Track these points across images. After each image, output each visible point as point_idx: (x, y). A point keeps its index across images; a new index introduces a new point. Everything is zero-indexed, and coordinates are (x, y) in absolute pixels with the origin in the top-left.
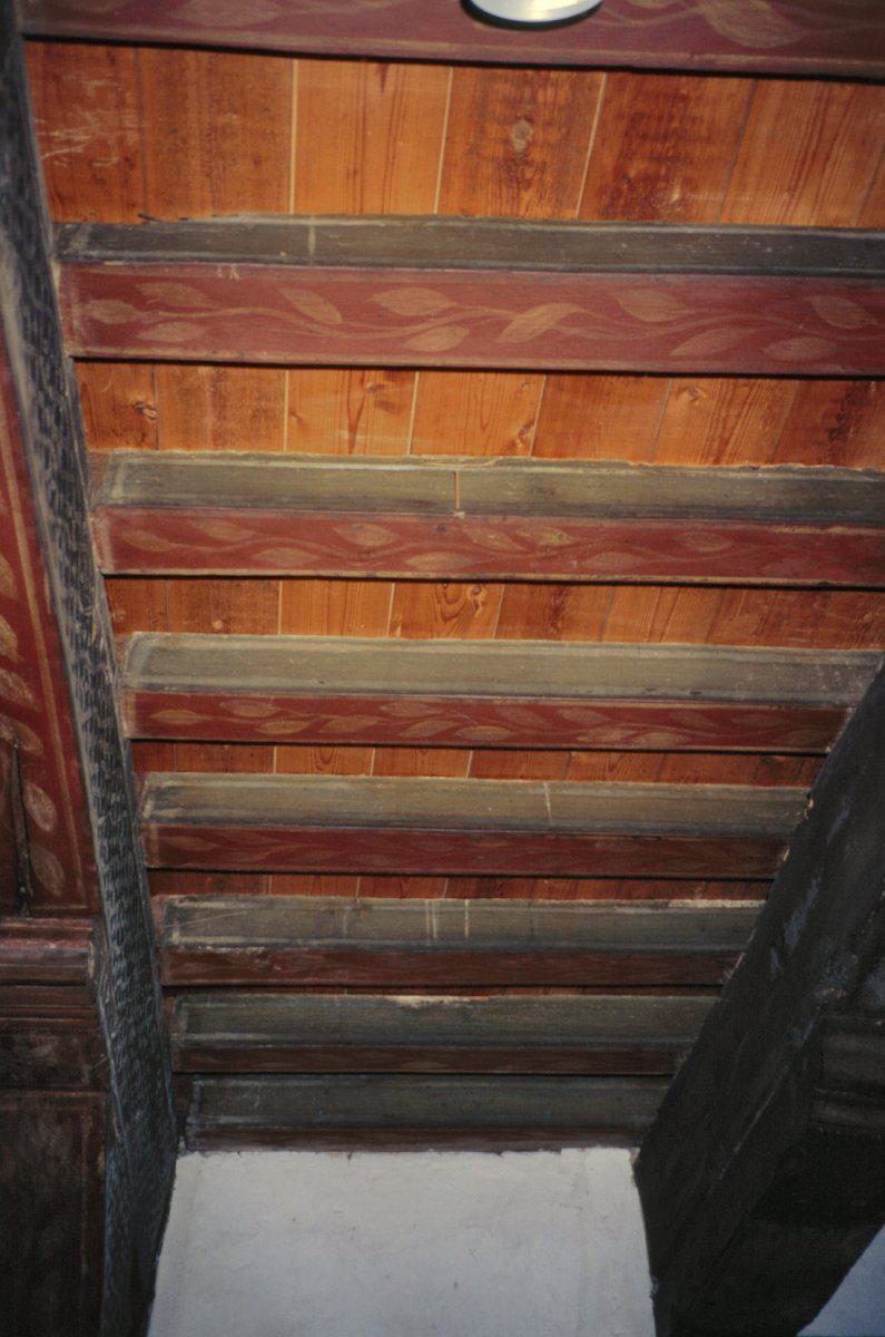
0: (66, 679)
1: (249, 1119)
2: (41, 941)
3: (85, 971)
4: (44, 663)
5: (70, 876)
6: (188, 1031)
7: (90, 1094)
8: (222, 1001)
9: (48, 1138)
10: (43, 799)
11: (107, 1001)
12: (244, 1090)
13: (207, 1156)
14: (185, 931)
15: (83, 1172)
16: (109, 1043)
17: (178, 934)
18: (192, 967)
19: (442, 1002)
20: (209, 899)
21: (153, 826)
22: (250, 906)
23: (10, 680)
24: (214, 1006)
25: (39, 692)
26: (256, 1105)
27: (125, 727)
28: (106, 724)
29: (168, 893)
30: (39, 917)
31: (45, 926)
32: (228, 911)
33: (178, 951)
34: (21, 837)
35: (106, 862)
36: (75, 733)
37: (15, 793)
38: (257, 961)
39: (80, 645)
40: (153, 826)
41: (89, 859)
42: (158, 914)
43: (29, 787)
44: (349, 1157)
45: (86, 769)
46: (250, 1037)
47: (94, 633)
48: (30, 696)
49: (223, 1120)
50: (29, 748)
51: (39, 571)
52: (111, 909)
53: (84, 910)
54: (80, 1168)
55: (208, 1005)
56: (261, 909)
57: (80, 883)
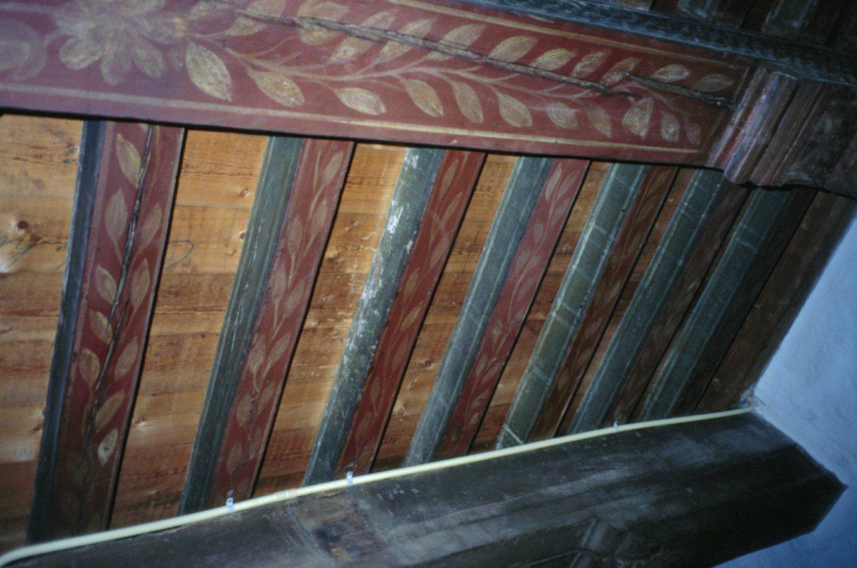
0: (598, 28)
2: (757, 103)
3: (791, 81)
4: (583, 37)
5: (722, 70)
10: (667, 70)
11: (817, 75)
16: (847, 84)
17: (795, 22)
21: (714, 13)
23: (586, 62)
25: (599, 47)
27: (642, 9)
28: (635, 18)
29: (764, 21)
30: (741, 100)
31: (749, 98)
34: (685, 92)
35: (725, 46)
36: (634, 34)
37: (655, 85)
39: (580, 14)
40: (714, 13)
41: (718, 55)
42: (775, 31)
43: (656, 75)
45: (659, 36)
47: (574, 5)
48: (600, 54)
50: (632, 67)
51: (528, 20)
52: (757, 54)
57: (731, 66)
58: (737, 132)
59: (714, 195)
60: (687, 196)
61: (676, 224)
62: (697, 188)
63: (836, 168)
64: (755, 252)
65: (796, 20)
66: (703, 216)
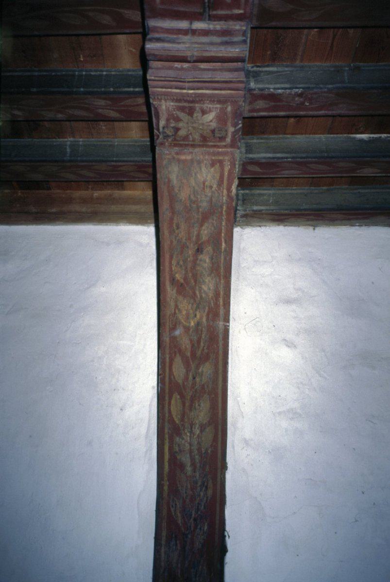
1: (268, 208)
6: (246, 153)
7: (229, 150)
8: (261, 139)
9: (207, 176)
12: (263, 195)
13: (244, 229)
14: (257, 82)
15: (224, 194)
17: (253, 83)
18: (261, 104)
19: (381, 137)
20: (268, 66)
22: (290, 69)
24: (258, 141)
26: (271, 202)
32: (277, 72)
33: (255, 92)
38: (297, 99)
44: (314, 229)
46: (279, 155)
49: (255, 208)
53: (241, 14)
54: (223, 192)
55: (255, 141)
56: (297, 70)
58: (185, 32)
59: (103, 89)
60: (92, 71)
61: (64, 73)
62: (101, 76)
63: (175, 148)
64: (65, 158)
65: (255, 84)
66: (82, 89)
